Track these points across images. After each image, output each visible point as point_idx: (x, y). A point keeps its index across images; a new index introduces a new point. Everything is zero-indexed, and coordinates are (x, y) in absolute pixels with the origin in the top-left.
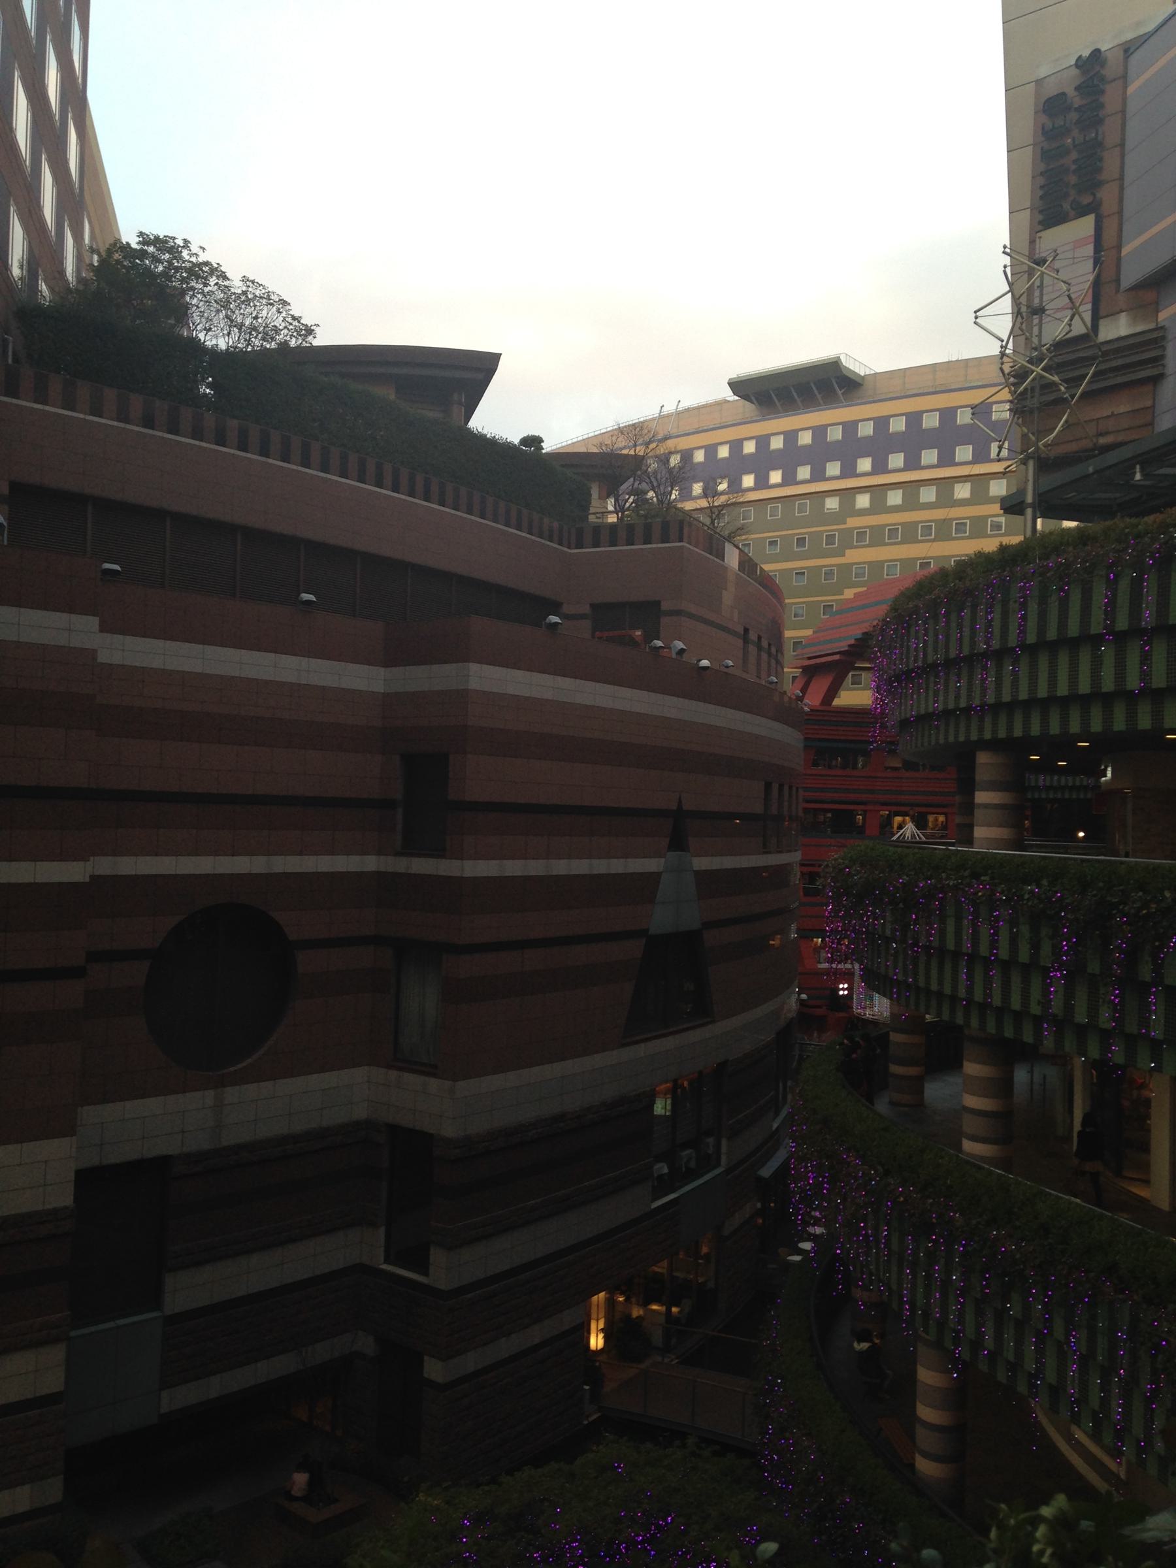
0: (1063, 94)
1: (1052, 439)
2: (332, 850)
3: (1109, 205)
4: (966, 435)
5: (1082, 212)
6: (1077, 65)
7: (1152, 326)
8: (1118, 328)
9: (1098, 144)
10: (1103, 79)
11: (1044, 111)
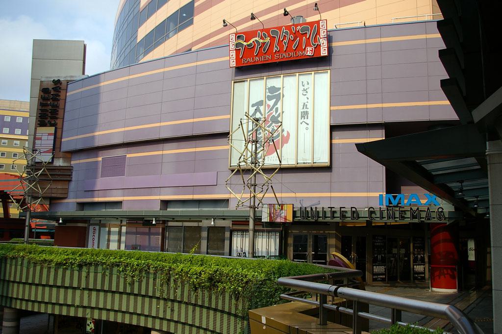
0: (48, 89)
1: (73, 250)
2: (208, 64)
3: (59, 126)
4: (19, 126)
5: (52, 125)
6: (53, 81)
7: (69, 165)
8: (59, 163)
9: (57, 107)
10: (60, 88)
11: (42, 92)
